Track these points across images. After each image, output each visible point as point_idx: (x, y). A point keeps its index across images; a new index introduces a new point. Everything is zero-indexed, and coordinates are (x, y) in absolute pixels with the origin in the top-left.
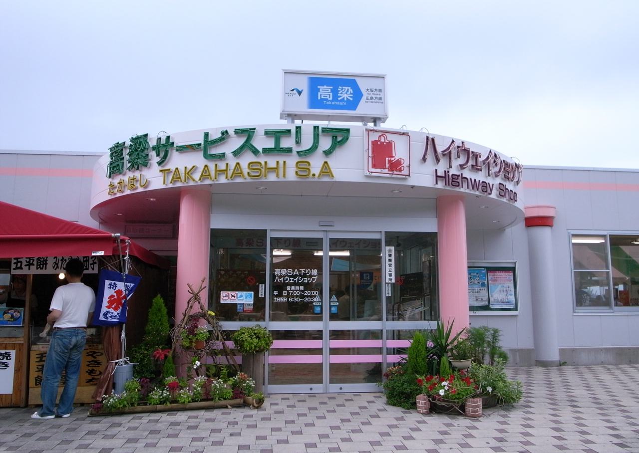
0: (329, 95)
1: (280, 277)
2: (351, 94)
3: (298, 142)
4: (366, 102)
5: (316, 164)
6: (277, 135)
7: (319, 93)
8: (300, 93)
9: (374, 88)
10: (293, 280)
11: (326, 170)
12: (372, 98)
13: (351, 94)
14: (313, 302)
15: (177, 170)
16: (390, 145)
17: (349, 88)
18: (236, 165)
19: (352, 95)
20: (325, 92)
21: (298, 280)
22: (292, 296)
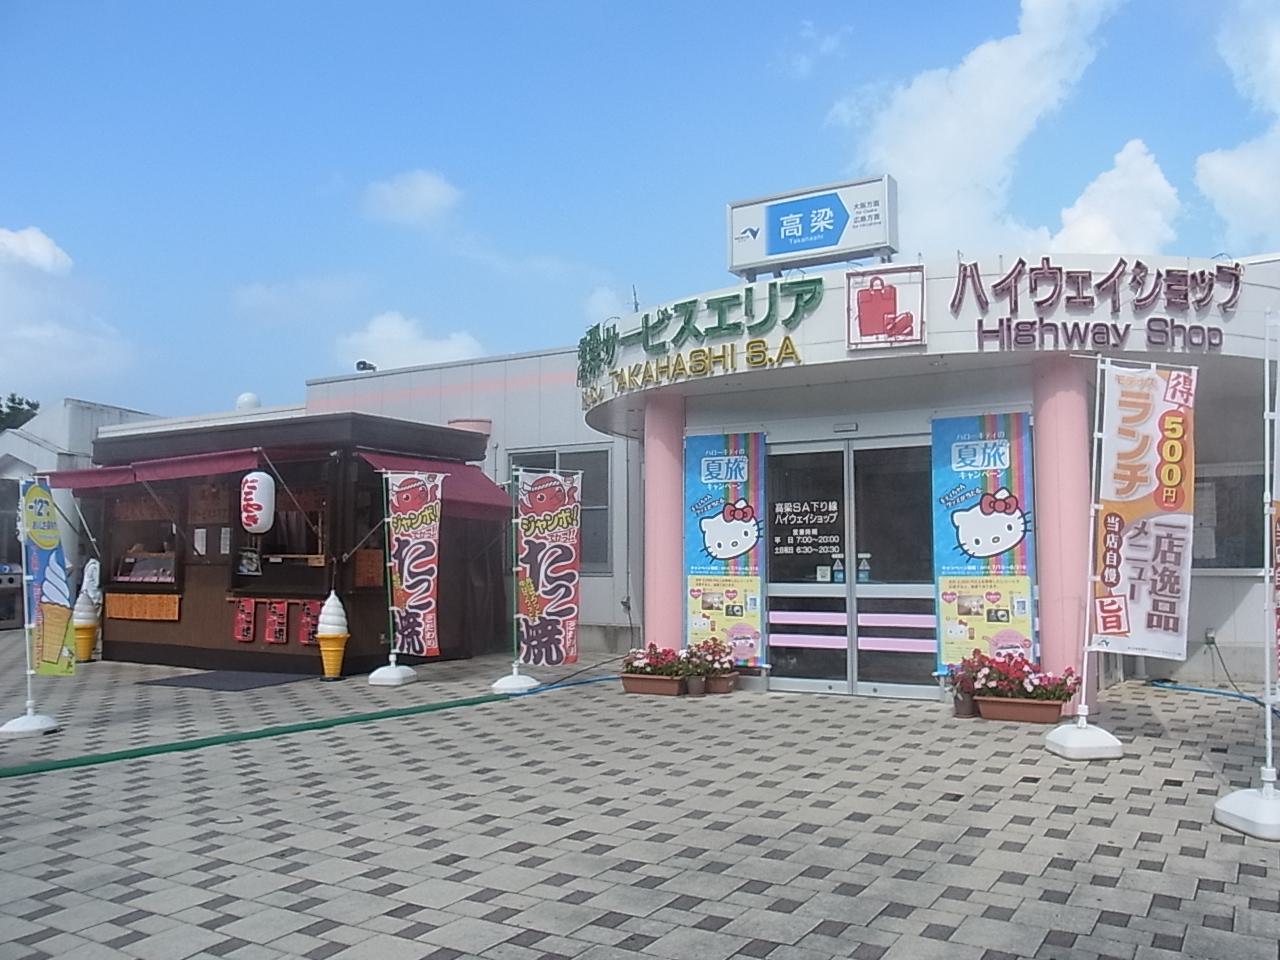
0: (798, 228)
1: (784, 515)
2: (830, 218)
3: (749, 313)
4: (854, 227)
5: (774, 340)
6: (720, 306)
7: (783, 229)
8: (754, 234)
9: (865, 200)
10: (802, 520)
11: (788, 351)
12: (863, 219)
13: (830, 218)
14: (831, 554)
15: (787, 341)
16: (890, 294)
17: (828, 210)
18: (784, 341)
19: (831, 221)
20: (791, 225)
21: (809, 520)
22: (801, 545)
